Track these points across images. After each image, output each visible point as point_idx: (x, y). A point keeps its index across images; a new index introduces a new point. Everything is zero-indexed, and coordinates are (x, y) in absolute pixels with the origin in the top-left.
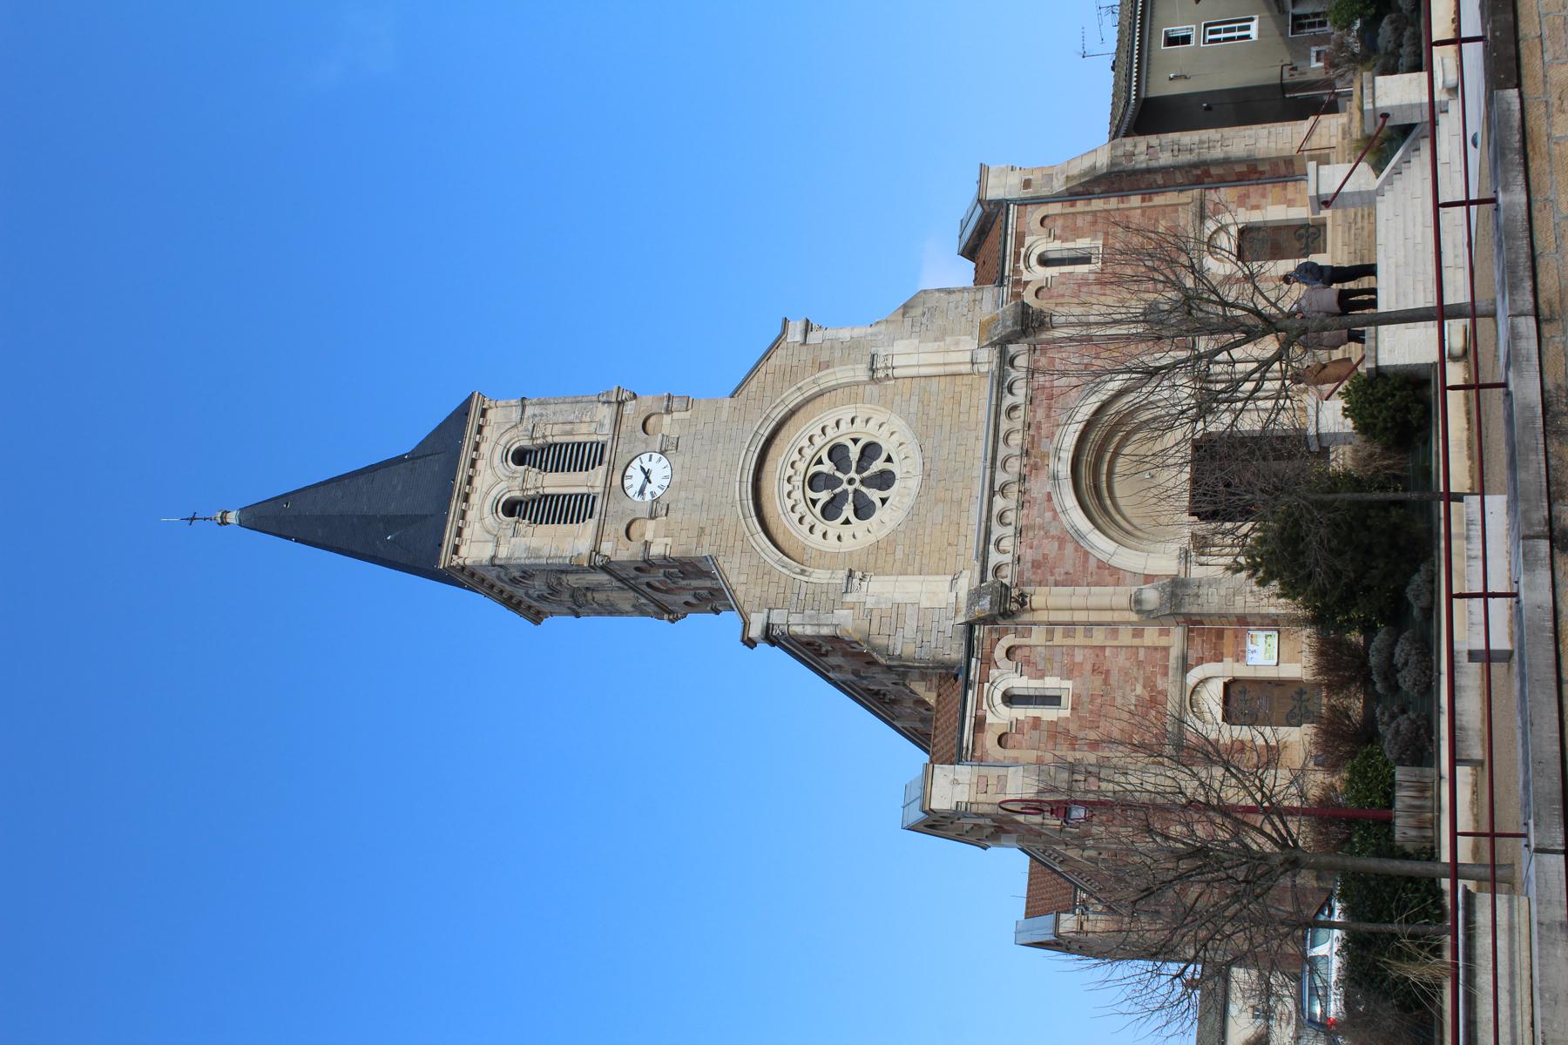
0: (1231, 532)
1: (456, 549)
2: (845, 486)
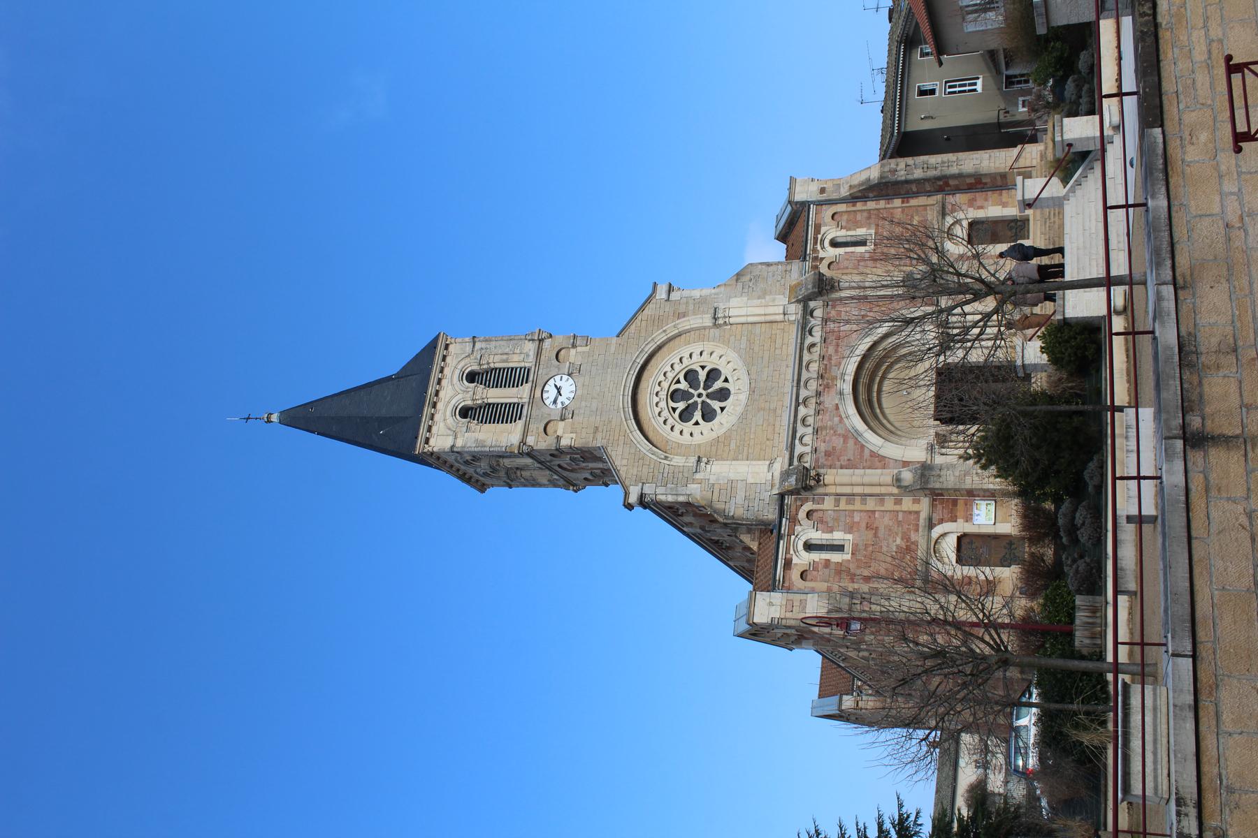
0: (963, 432)
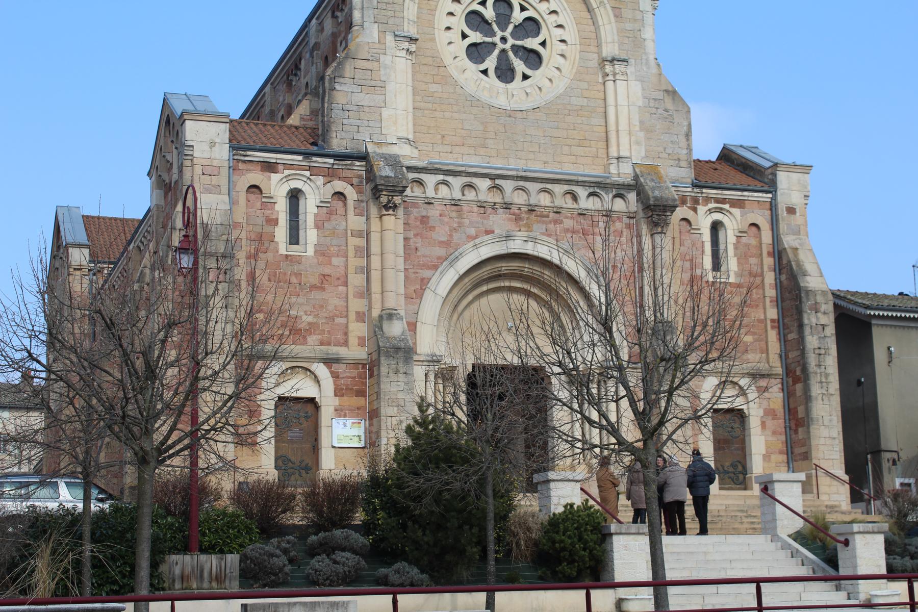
0: (457, 401)
2: (499, 34)
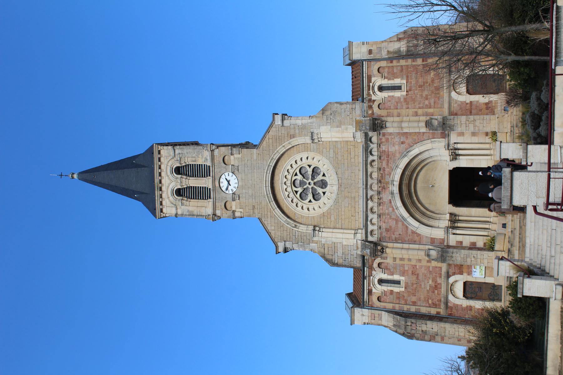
1: (161, 211)
2: (307, 185)
